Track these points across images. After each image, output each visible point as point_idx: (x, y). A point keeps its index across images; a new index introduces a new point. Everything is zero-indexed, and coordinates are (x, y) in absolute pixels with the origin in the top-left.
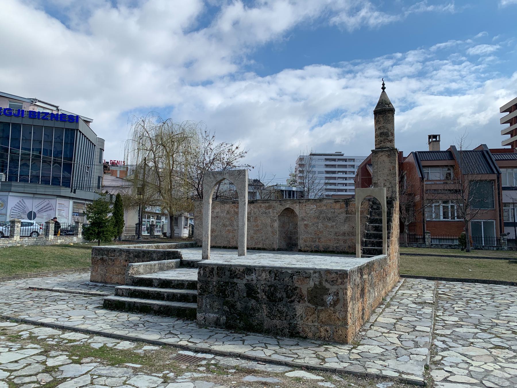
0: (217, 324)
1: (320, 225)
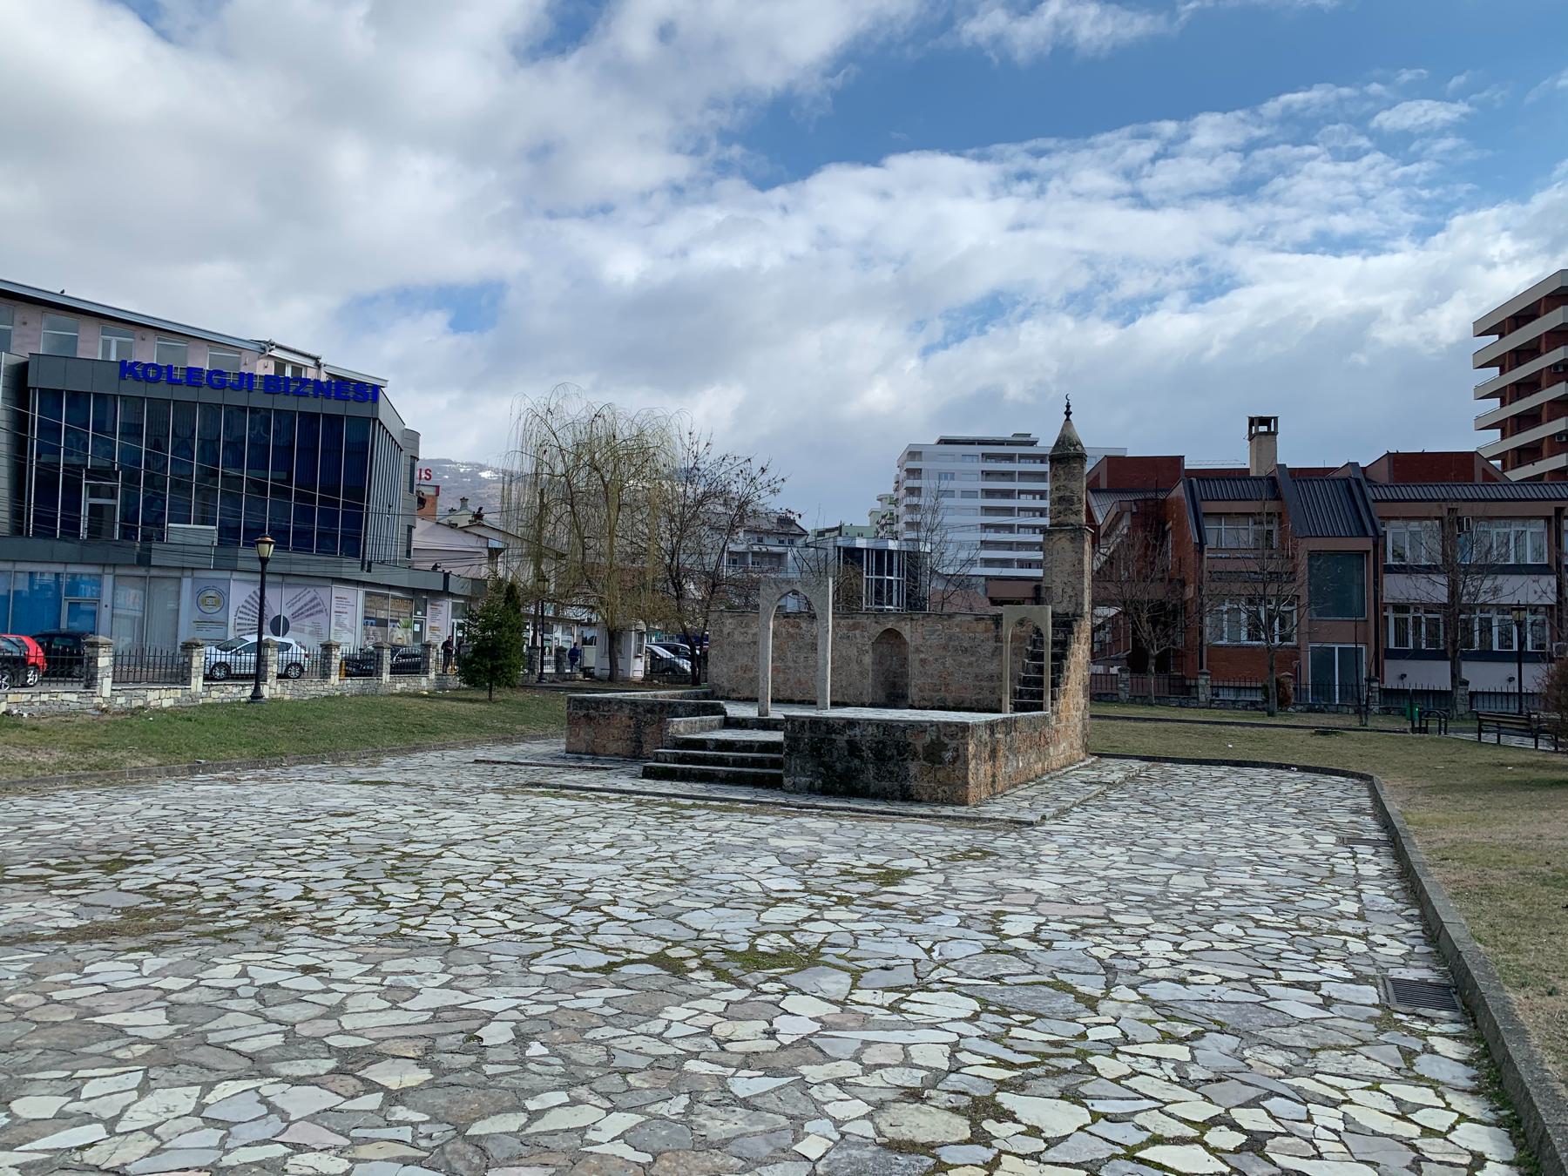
0: (811, 790)
1: (949, 661)
